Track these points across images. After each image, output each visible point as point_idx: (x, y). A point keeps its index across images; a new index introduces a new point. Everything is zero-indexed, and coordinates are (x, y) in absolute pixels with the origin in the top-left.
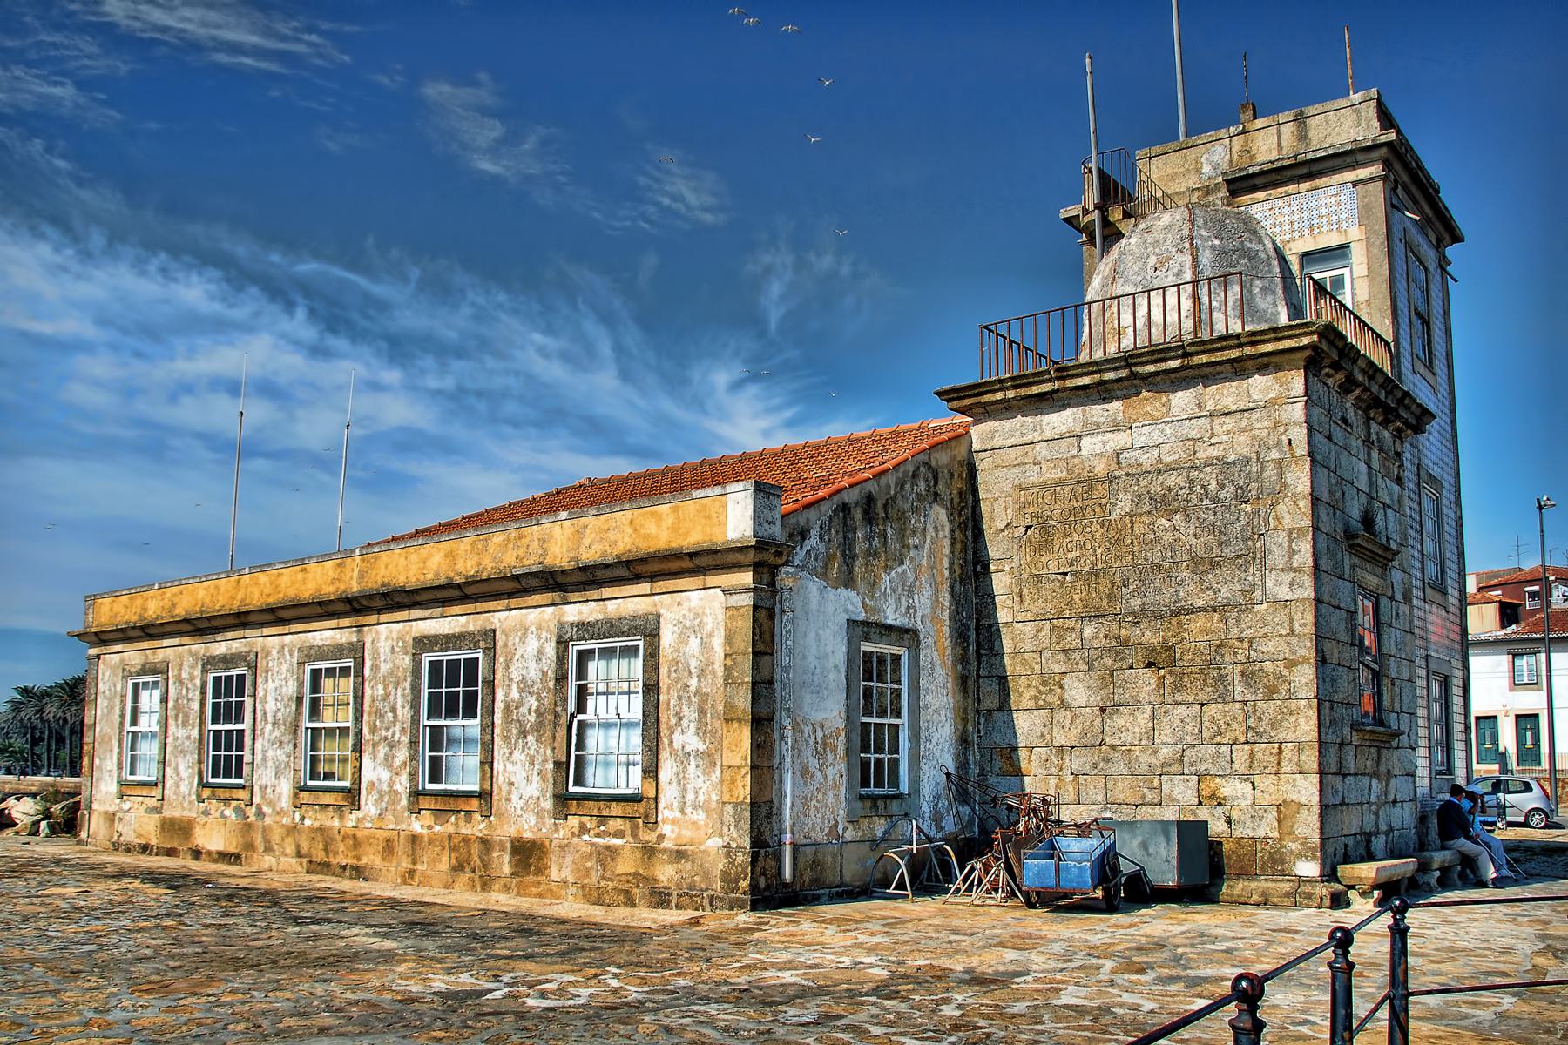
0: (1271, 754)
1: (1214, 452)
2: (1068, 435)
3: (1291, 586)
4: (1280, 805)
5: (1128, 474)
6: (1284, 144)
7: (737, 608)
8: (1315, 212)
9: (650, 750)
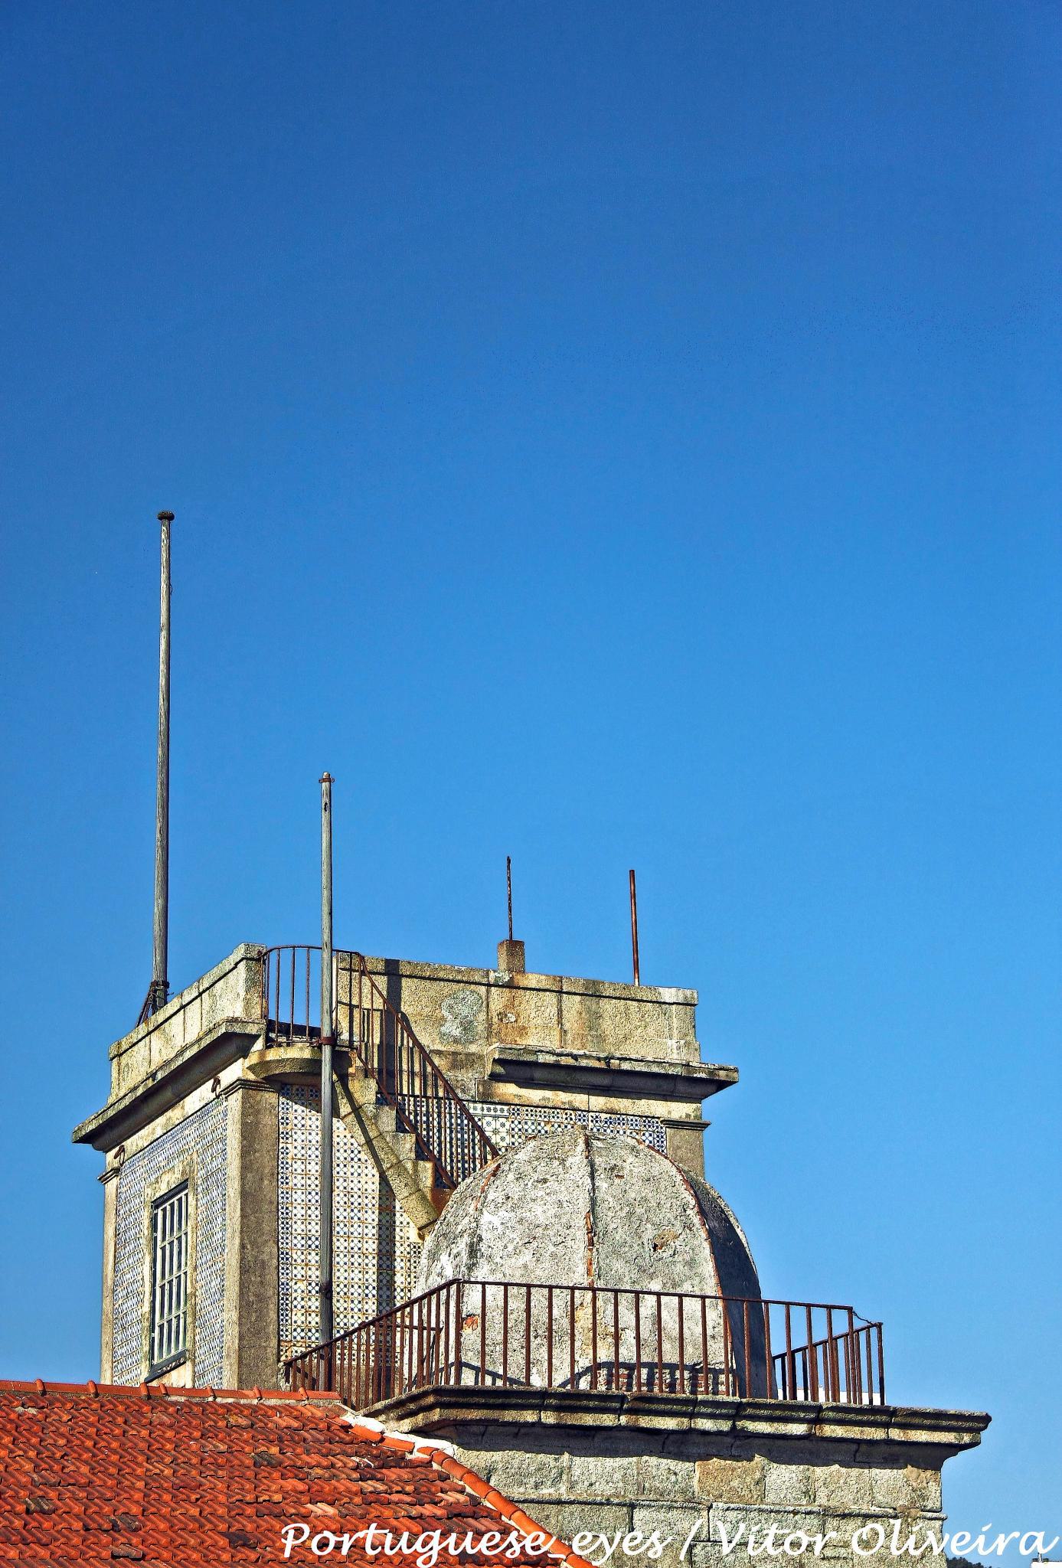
2: (616, 1501)
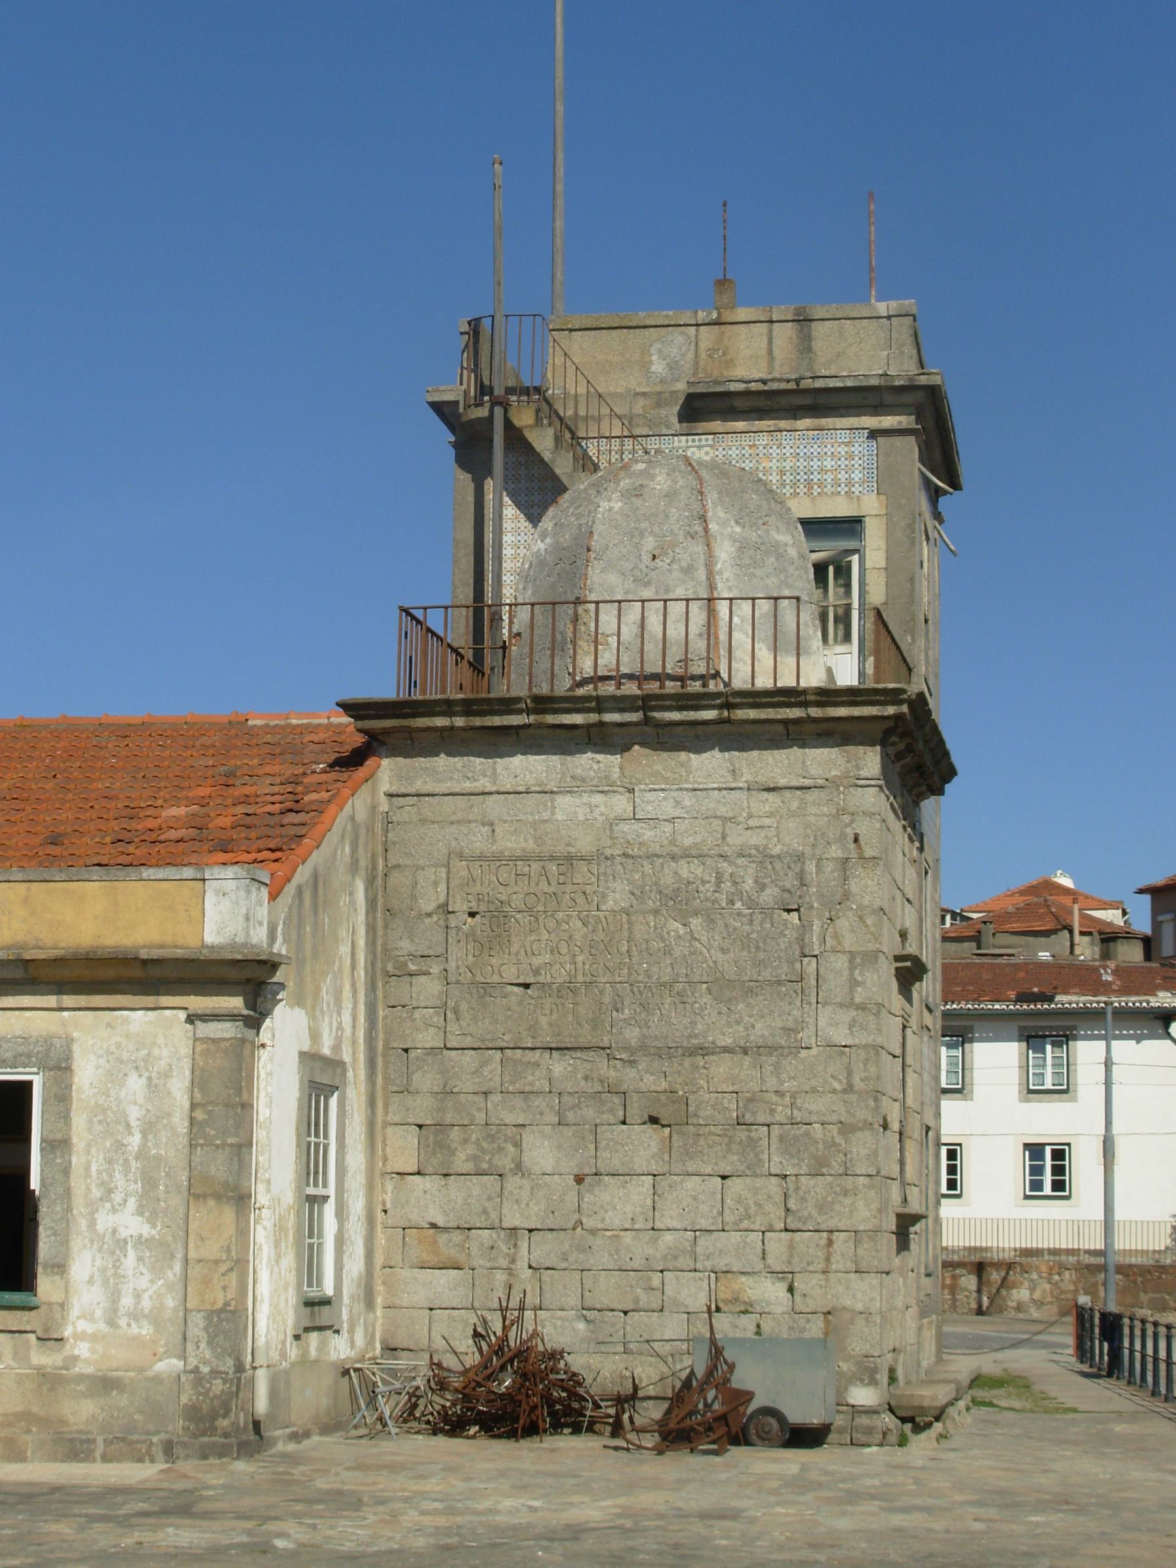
0: (818, 1246)
1: (755, 839)
2: (537, 789)
3: (851, 1027)
4: (829, 1313)
5: (625, 855)
6: (777, 352)
7: (214, 1041)
8: (815, 464)
9: (55, 1234)
